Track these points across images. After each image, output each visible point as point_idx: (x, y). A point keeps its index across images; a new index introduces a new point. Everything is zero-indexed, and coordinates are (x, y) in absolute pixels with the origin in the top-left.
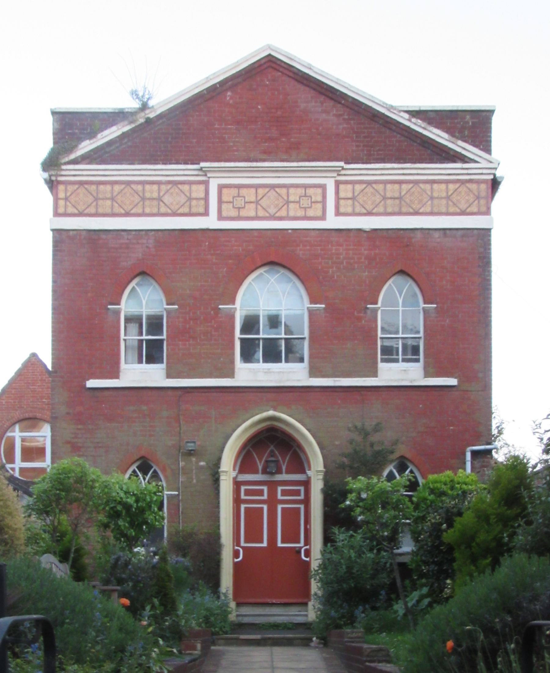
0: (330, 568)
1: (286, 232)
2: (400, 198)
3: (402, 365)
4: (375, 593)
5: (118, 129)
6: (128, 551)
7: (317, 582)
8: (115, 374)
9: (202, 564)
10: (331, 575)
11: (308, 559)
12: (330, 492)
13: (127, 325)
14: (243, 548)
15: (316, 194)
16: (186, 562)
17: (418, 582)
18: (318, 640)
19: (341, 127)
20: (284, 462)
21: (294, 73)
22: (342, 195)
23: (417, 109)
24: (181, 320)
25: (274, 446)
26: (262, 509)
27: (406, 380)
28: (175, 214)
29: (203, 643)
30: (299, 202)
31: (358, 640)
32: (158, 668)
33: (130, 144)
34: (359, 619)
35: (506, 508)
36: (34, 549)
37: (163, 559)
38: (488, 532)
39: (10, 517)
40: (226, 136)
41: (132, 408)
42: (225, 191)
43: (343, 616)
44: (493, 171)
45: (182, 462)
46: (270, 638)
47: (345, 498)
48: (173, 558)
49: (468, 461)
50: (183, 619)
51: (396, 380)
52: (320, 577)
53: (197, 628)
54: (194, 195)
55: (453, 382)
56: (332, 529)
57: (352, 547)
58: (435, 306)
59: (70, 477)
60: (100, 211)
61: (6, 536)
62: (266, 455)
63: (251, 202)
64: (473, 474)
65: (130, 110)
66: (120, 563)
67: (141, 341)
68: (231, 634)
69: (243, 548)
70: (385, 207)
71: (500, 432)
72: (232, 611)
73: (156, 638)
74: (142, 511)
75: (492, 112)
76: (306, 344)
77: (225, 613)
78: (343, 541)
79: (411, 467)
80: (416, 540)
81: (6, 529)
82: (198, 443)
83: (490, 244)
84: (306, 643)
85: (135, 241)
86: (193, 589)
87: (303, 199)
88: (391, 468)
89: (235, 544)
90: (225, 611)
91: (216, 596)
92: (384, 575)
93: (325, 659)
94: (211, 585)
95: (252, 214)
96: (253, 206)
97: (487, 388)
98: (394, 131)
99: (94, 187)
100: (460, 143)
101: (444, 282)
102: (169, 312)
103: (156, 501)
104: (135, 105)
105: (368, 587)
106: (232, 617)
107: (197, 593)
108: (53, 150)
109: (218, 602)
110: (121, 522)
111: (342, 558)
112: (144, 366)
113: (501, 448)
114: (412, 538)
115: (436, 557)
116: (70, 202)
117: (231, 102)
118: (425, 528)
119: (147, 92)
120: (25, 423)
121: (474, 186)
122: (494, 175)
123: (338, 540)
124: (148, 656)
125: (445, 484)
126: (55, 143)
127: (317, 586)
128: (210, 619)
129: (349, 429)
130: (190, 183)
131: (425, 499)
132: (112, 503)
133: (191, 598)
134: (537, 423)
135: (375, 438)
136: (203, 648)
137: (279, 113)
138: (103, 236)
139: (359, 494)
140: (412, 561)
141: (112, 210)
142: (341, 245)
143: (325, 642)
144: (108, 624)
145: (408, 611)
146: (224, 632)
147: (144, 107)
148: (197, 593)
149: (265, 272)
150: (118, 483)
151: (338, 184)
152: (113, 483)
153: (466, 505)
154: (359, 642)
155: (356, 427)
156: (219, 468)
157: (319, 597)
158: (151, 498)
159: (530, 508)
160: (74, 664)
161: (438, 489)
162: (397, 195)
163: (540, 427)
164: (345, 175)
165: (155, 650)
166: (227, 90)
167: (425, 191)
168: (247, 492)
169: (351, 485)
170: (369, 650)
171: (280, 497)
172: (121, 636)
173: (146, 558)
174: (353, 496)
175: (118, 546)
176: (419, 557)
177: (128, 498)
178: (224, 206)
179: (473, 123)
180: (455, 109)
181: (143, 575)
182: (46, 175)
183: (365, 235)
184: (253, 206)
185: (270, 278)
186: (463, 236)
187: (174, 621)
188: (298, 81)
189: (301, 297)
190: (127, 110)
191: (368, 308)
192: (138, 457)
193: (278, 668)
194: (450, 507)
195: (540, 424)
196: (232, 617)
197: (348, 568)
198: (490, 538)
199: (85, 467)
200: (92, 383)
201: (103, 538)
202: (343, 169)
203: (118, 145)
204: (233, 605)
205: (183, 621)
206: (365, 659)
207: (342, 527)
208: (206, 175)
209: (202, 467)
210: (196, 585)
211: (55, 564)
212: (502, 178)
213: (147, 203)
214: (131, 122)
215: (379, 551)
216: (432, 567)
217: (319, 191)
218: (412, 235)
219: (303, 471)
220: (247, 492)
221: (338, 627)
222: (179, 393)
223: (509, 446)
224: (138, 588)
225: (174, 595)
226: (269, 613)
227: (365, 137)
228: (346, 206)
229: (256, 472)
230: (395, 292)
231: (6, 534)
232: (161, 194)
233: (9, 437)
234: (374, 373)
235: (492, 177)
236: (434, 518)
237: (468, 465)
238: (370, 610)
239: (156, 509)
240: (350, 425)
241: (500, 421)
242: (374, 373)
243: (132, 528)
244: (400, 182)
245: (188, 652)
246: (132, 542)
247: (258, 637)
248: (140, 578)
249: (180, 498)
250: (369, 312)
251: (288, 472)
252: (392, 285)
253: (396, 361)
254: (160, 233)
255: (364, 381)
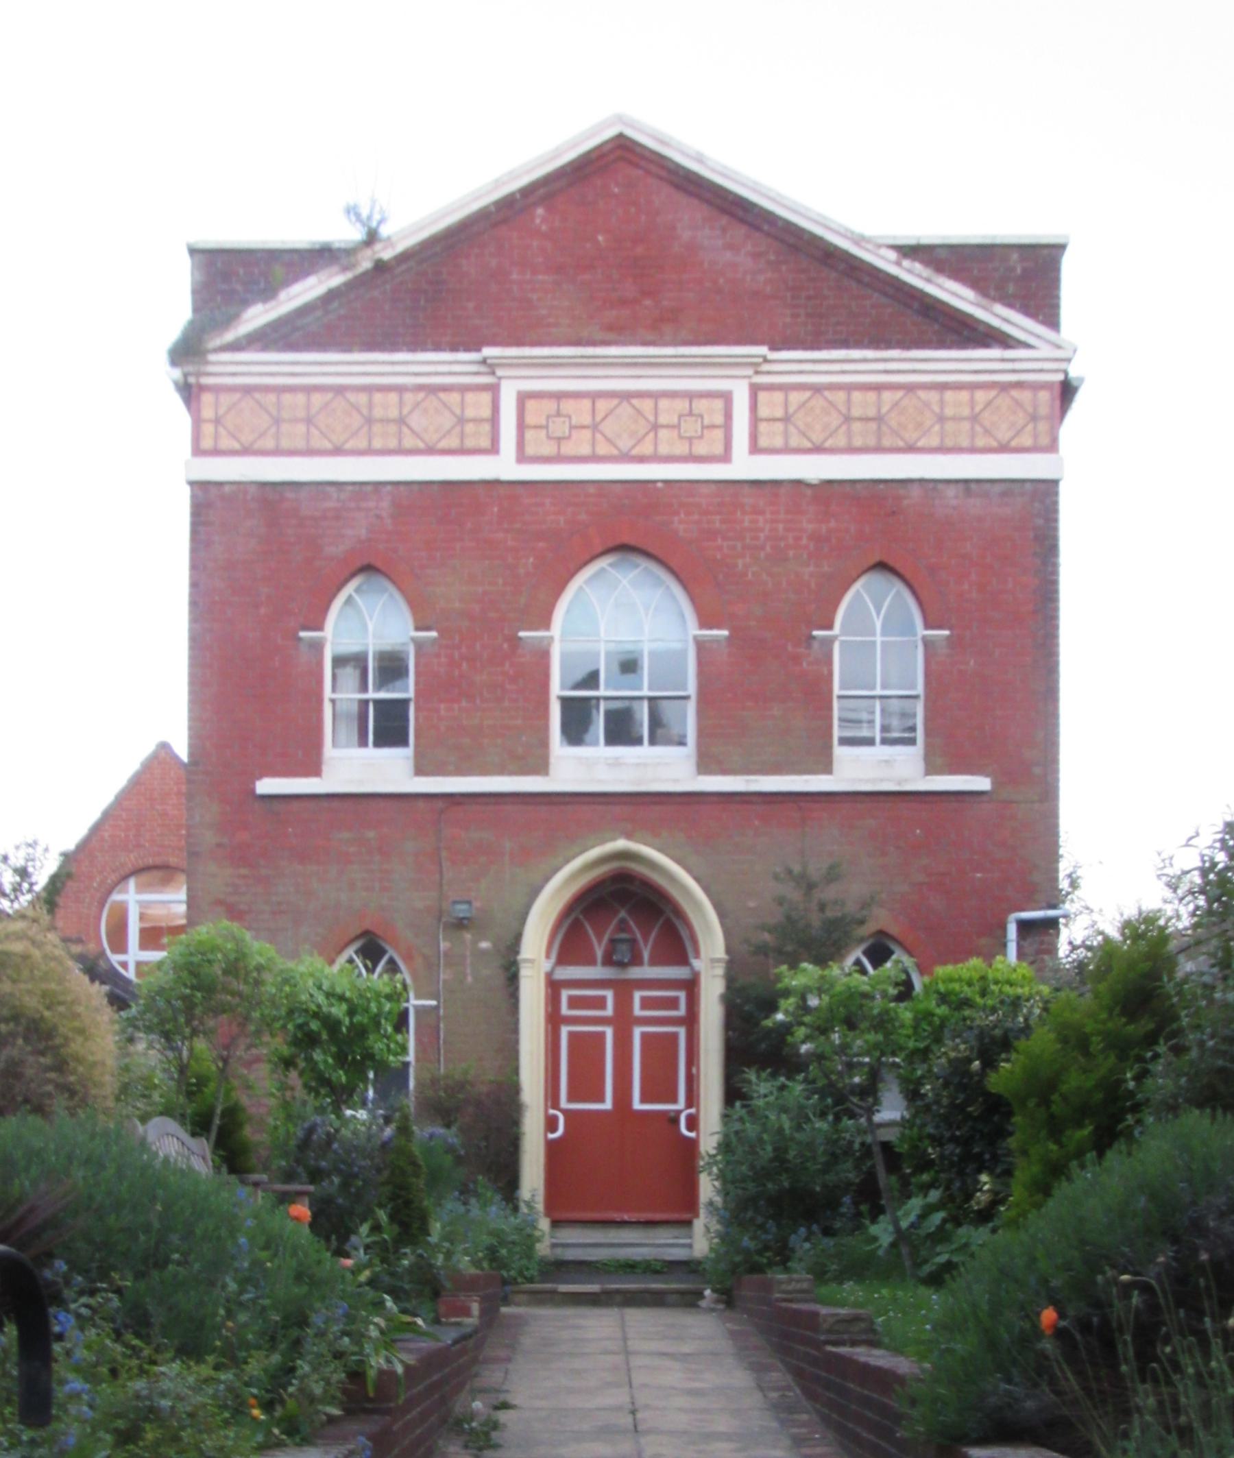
0: (740, 1150)
1: (650, 486)
2: (879, 419)
3: (880, 751)
4: (831, 1202)
5: (320, 282)
6: (333, 1112)
7: (713, 1180)
8: (313, 767)
9: (483, 1144)
10: (742, 1164)
11: (692, 1135)
12: (738, 1001)
13: (336, 671)
14: (565, 1112)
15: (713, 411)
16: (451, 1136)
17: (913, 1180)
18: (715, 1295)
19: (761, 278)
20: (646, 945)
21: (669, 171)
22: (763, 412)
23: (913, 242)
24: (443, 660)
25: (630, 912)
26: (602, 1036)
27: (889, 780)
28: (431, 451)
29: (484, 1300)
30: (677, 427)
31: (799, 1296)
32: (382, 1361)
33: (342, 312)
34: (799, 1254)
35: (1124, 1020)
36: (138, 1109)
37: (404, 1130)
38: (1085, 1071)
39: (80, 1039)
40: (535, 297)
41: (346, 835)
42: (531, 405)
43: (766, 1248)
44: (1063, 366)
45: (445, 939)
46: (618, 1291)
47: (773, 1007)
48: (423, 1131)
49: (1012, 941)
50: (439, 1252)
51: (868, 781)
52: (720, 1170)
53: (473, 1271)
54: (470, 413)
55: (981, 783)
56: (744, 1072)
57: (784, 1109)
58: (946, 633)
59: (214, 961)
60: (285, 444)
61: (72, 1078)
62: (612, 927)
63: (583, 427)
64: (1024, 964)
65: (343, 245)
66: (315, 1137)
67: (364, 703)
68: (543, 1282)
69: (565, 1112)
70: (849, 435)
71: (1074, 884)
72: (543, 1236)
73: (379, 1294)
74: (360, 1033)
75: (1061, 248)
76: (691, 708)
77: (529, 1241)
78: (765, 1096)
79: (899, 955)
80: (912, 1094)
81: (72, 1064)
82: (477, 904)
83: (1056, 511)
84: (690, 1300)
85: (353, 505)
86: (466, 1191)
87: (685, 421)
88: (857, 953)
89: (549, 1104)
90: (529, 1236)
91: (511, 1205)
92: (849, 1165)
93: (733, 1335)
94: (500, 1185)
95: (585, 450)
96: (587, 434)
97: (1048, 793)
98: (868, 285)
99: (272, 398)
100: (999, 309)
101: (966, 587)
102: (419, 645)
103: (390, 1013)
104: (355, 234)
105: (818, 1189)
106: (543, 1249)
107: (473, 1201)
108: (192, 323)
109: (516, 1218)
110: (318, 1055)
111: (765, 1130)
112: (371, 752)
113: (1076, 916)
114: (901, 1092)
115: (959, 1128)
116: (225, 428)
117: (544, 228)
118: (935, 1070)
119: (377, 208)
120: (145, 877)
121: (1025, 396)
122: (1066, 373)
123: (755, 1095)
124: (358, 1338)
125: (970, 984)
126: (196, 309)
127: (714, 1186)
128: (498, 1251)
129: (776, 877)
130: (464, 389)
131: (929, 1015)
132: (300, 1016)
133: (462, 1209)
134: (1164, 855)
135: (830, 893)
136: (483, 1312)
137: (640, 250)
138: (290, 495)
139: (804, 999)
140: (903, 1138)
141: (308, 441)
142: (762, 513)
143: (728, 1298)
144: (269, 1264)
145: (901, 1236)
146: (525, 1278)
147: (372, 237)
148: (473, 1201)
149: (611, 565)
150: (312, 975)
151: (755, 390)
152: (302, 975)
153: (1020, 1023)
154: (806, 1301)
155: (790, 872)
156: (517, 953)
157: (717, 1209)
158: (380, 1006)
159: (1187, 1016)
160: (173, 1360)
161: (956, 994)
162: (871, 412)
163: (1171, 865)
164: (769, 373)
165: (376, 1320)
166: (535, 205)
167: (927, 405)
168: (574, 1002)
169: (786, 980)
170: (831, 1320)
171: (637, 1011)
172: (299, 1290)
173: (369, 1128)
174: (789, 1003)
175: (311, 1100)
176: (915, 1130)
177: (331, 1005)
178: (529, 435)
179: (1024, 270)
180: (988, 241)
181: (363, 1163)
182: (177, 373)
183: (809, 492)
184: (587, 434)
185: (619, 577)
186: (1004, 494)
187: (421, 1256)
188: (678, 187)
189: (682, 616)
190: (337, 245)
191: (814, 638)
192: (359, 931)
193: (637, 1353)
194: (988, 1025)
195: (1171, 858)
196: (543, 1249)
197: (775, 1149)
198: (1090, 1084)
199: (243, 941)
200: (267, 786)
201: (284, 1087)
202: (766, 360)
203: (319, 313)
204: (544, 1224)
205: (441, 1257)
206: (822, 1338)
207: (764, 1069)
208: (493, 373)
209: (484, 952)
210: (471, 1186)
211: (178, 1139)
212: (1081, 380)
213: (377, 428)
214: (345, 269)
215: (837, 1119)
216: (949, 1148)
217: (719, 404)
218: (901, 492)
219: (683, 960)
220: (574, 1002)
221: (756, 1269)
222: (440, 804)
223: (1092, 911)
224: (353, 1190)
225: (426, 1203)
226: (616, 1241)
227: (809, 298)
228: (771, 434)
229: (591, 961)
230: (868, 609)
231: (72, 1074)
232: (405, 411)
233: (115, 902)
234: (826, 767)
235: (1061, 377)
236: (954, 1048)
237: (1012, 948)
238: (820, 1236)
239: (390, 1029)
240: (778, 870)
241: (1073, 864)
242: (826, 767)
243: (342, 1068)
244: (878, 388)
245: (453, 1320)
246: (343, 1095)
247: (594, 1288)
248: (356, 1169)
249: (442, 1012)
250: (816, 645)
251: (655, 961)
252: (862, 591)
253: (869, 742)
254: (402, 488)
255: (806, 781)
